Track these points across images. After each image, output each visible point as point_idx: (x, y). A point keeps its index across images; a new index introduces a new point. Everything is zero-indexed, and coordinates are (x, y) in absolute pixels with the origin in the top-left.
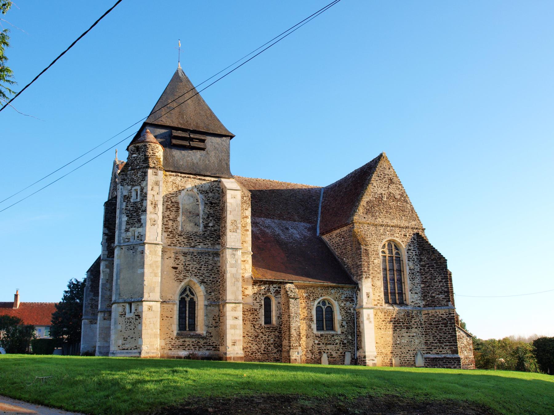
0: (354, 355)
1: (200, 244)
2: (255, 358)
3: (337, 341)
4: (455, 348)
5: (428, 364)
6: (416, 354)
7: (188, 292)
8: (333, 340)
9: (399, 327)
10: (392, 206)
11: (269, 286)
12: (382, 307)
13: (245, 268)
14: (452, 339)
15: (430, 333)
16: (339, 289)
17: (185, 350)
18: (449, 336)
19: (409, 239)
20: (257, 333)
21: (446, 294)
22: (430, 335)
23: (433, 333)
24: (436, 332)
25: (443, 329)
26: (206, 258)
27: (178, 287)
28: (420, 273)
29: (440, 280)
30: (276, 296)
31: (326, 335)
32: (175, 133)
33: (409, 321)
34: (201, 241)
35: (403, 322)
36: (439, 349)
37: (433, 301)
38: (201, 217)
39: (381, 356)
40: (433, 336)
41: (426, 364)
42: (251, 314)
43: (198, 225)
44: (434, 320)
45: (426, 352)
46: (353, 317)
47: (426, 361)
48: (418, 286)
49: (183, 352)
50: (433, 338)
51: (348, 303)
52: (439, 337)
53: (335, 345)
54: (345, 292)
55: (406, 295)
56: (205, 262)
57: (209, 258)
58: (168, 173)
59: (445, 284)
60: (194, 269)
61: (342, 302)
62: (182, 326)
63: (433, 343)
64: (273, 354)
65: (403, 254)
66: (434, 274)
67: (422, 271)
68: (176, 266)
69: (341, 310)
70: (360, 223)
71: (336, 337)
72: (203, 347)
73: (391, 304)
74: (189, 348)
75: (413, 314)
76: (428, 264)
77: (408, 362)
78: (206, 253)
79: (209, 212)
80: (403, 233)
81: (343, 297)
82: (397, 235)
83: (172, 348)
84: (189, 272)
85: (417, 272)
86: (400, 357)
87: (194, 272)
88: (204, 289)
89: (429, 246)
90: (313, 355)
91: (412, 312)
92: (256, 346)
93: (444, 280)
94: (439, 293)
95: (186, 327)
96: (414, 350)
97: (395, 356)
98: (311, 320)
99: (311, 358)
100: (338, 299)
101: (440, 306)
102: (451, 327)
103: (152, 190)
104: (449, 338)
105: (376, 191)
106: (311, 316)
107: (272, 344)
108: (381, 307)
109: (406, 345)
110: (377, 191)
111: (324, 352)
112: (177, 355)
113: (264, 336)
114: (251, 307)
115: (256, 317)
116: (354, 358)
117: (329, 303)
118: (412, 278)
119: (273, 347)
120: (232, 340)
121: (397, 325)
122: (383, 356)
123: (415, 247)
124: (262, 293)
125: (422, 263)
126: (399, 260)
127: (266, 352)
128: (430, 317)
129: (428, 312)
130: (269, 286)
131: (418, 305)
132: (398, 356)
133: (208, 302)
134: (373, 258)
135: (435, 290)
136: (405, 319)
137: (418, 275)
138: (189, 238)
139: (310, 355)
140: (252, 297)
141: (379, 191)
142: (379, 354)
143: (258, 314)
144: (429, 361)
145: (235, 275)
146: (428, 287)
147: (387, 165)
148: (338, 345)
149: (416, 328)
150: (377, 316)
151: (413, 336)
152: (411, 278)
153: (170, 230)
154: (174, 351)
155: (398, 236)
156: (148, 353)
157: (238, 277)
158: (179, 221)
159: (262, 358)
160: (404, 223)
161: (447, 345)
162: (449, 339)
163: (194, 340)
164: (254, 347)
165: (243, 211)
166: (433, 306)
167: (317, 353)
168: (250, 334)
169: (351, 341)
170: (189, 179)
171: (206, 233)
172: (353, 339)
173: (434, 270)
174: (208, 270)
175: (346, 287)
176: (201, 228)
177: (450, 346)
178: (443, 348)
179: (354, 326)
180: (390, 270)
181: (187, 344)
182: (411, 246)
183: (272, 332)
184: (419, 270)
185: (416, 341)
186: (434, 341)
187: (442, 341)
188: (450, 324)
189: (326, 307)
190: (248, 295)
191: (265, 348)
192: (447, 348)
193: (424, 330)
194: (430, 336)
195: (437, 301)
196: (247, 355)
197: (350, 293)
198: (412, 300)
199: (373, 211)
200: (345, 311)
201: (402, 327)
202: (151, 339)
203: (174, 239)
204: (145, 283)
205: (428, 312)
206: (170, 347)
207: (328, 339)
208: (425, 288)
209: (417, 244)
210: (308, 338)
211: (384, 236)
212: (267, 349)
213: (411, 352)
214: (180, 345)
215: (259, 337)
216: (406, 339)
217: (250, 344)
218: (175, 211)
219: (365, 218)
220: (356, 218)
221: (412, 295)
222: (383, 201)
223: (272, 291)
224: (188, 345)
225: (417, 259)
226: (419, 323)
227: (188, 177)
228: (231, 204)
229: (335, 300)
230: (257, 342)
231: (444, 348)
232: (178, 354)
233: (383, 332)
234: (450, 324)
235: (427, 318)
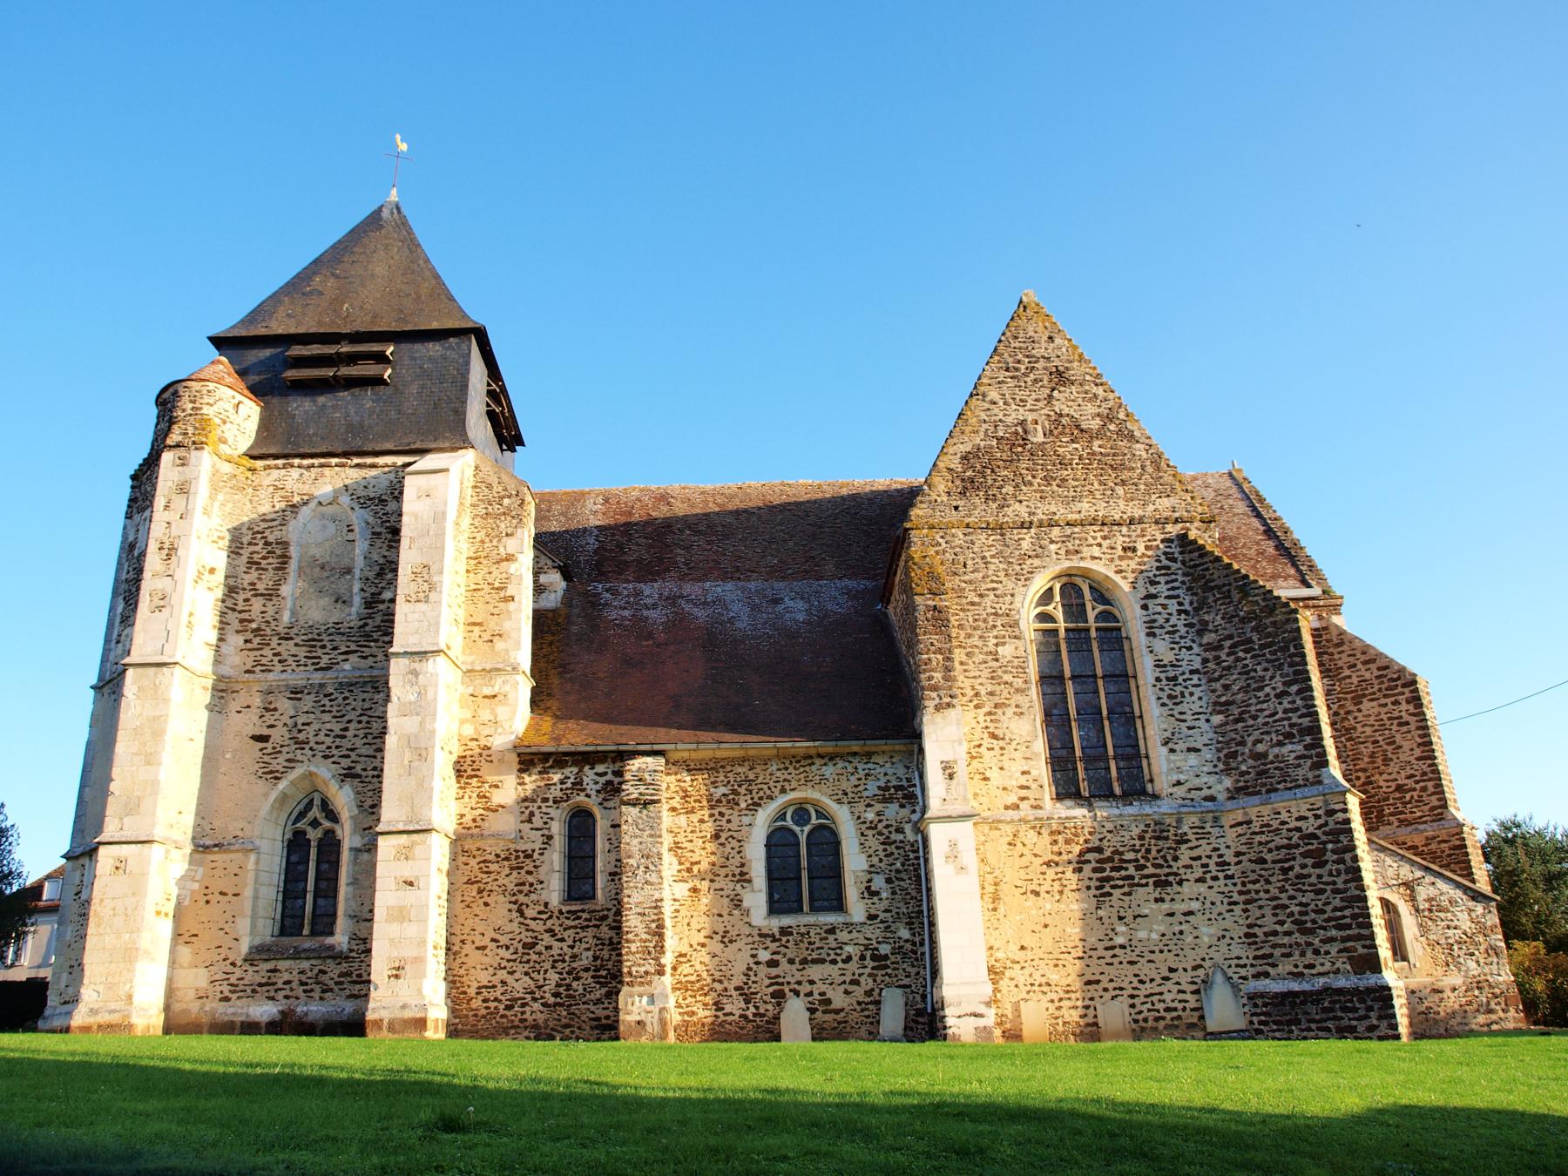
0: (924, 997)
1: (350, 657)
2: (522, 1021)
3: (849, 949)
4: (1364, 947)
5: (1263, 1018)
6: (1203, 981)
7: (315, 812)
8: (834, 945)
9: (1120, 883)
10: (1069, 457)
11: (580, 771)
12: (1040, 813)
13: (496, 717)
14: (1347, 912)
15: (1262, 894)
16: (856, 761)
17: (272, 998)
18: (1337, 903)
19: (1146, 559)
20: (530, 934)
21: (1308, 739)
22: (1260, 903)
23: (1272, 894)
24: (1282, 890)
25: (1309, 876)
26: (364, 700)
27: (266, 795)
28: (1205, 673)
29: (1280, 688)
30: (605, 804)
31: (803, 930)
32: (297, 351)
33: (1164, 857)
34: (353, 647)
35: (1136, 860)
36: (1303, 954)
37: (1260, 774)
38: (357, 577)
39: (1045, 999)
40: (1275, 908)
41: (1255, 1019)
42: (512, 869)
43: (344, 602)
44: (1272, 845)
45: (1252, 971)
46: (912, 855)
47: (1256, 1005)
48: (1202, 723)
49: (265, 1008)
50: (1275, 915)
51: (894, 807)
52: (1296, 909)
53: (840, 965)
54: (878, 770)
55: (1152, 761)
56: (360, 712)
57: (376, 696)
58: (259, 464)
59: (1299, 702)
60: (321, 738)
61: (869, 805)
62: (289, 923)
63: (1275, 933)
64: (593, 1008)
65: (1128, 614)
66: (1255, 671)
67: (1211, 665)
68: (266, 732)
69: (862, 834)
70: (932, 527)
71: (843, 936)
72: (336, 988)
73: (1087, 799)
74: (288, 992)
75: (1185, 828)
76: (1230, 637)
77: (1169, 1016)
78: (366, 683)
79: (385, 557)
80: (1120, 541)
81: (872, 788)
82: (1096, 551)
83: (230, 995)
84: (307, 747)
85: (1192, 672)
86: (1132, 997)
87: (323, 747)
88: (352, 796)
89: (1225, 572)
90: (750, 1006)
91: (1179, 821)
92: (527, 978)
93: (1294, 688)
94: (1281, 738)
95: (302, 926)
96: (1195, 968)
97: (1107, 996)
98: (743, 878)
99: (741, 1016)
100: (850, 795)
101: (1290, 789)
102: (1341, 867)
103: (166, 507)
104: (1335, 909)
105: (1001, 417)
106: (743, 865)
107: (587, 970)
108: (1034, 811)
109: (1157, 949)
110: (1005, 415)
111: (797, 993)
112: (243, 1018)
113: (556, 944)
114: (512, 846)
115: (530, 879)
116: (926, 1009)
117: (820, 815)
118: (1170, 697)
119: (590, 980)
120: (389, 958)
121: (1113, 874)
122: (1055, 996)
123: (1176, 584)
124: (551, 797)
125: (1209, 638)
126: (1113, 637)
127: (564, 997)
128: (1254, 833)
129: (1246, 814)
130: (580, 771)
131: (1206, 792)
132: (1124, 992)
133: (363, 838)
134: (995, 641)
135: (1265, 729)
136: (1148, 851)
137: (1196, 681)
138: (312, 643)
139: (735, 1006)
140: (517, 809)
141: (1013, 416)
142: (1036, 988)
143: (535, 867)
144: (1265, 1005)
145: (412, 739)
146: (1237, 721)
147: (1040, 329)
148: (853, 966)
149: (1200, 880)
150: (1019, 845)
151: (1191, 913)
152: (1164, 695)
153: (254, 626)
154: (238, 1003)
155: (1096, 555)
156: (93, 1012)
157: (423, 746)
158: (283, 595)
159: (546, 1020)
160: (1120, 509)
161: (1331, 940)
162: (1339, 914)
163: (305, 965)
164: (520, 985)
165: (499, 541)
166: (1264, 790)
167: (768, 998)
168: (504, 940)
169: (908, 946)
170: (327, 471)
171: (370, 621)
172: (917, 939)
173: (1252, 657)
174: (370, 737)
175: (883, 752)
176: (354, 610)
177: (1344, 939)
178: (1317, 952)
179: (920, 891)
180: (1073, 678)
181: (281, 981)
182: (1159, 583)
183: (588, 926)
184: (1197, 665)
185: (1204, 929)
186: (1278, 928)
187: (1309, 925)
188: (1334, 852)
189: (807, 829)
190: (503, 807)
191: (558, 985)
192: (1334, 951)
193: (1239, 887)
194: (1260, 907)
195: (1276, 769)
196: (491, 1013)
197: (901, 772)
198: (1175, 778)
199: (990, 482)
200: (882, 838)
201: (1136, 881)
202: (114, 965)
203: (267, 652)
204: (113, 787)
205: (1246, 814)
206: (226, 989)
207: (810, 943)
208: (1228, 728)
209: (1184, 575)
210: (731, 942)
211: (1036, 562)
212: (569, 987)
213: (1184, 978)
214: (260, 985)
215: (539, 948)
216: (1155, 927)
217: (504, 972)
218: (277, 569)
219: (956, 508)
220: (920, 512)
221: (1172, 757)
222: (1029, 447)
223: (591, 788)
224: (285, 983)
225: (1185, 625)
226: (1212, 862)
227: (322, 466)
228: (416, 517)
229: (839, 801)
230: (532, 964)
231: (1322, 951)
232: (247, 1015)
233: (1048, 906)
234: (1334, 852)
235: (1243, 840)
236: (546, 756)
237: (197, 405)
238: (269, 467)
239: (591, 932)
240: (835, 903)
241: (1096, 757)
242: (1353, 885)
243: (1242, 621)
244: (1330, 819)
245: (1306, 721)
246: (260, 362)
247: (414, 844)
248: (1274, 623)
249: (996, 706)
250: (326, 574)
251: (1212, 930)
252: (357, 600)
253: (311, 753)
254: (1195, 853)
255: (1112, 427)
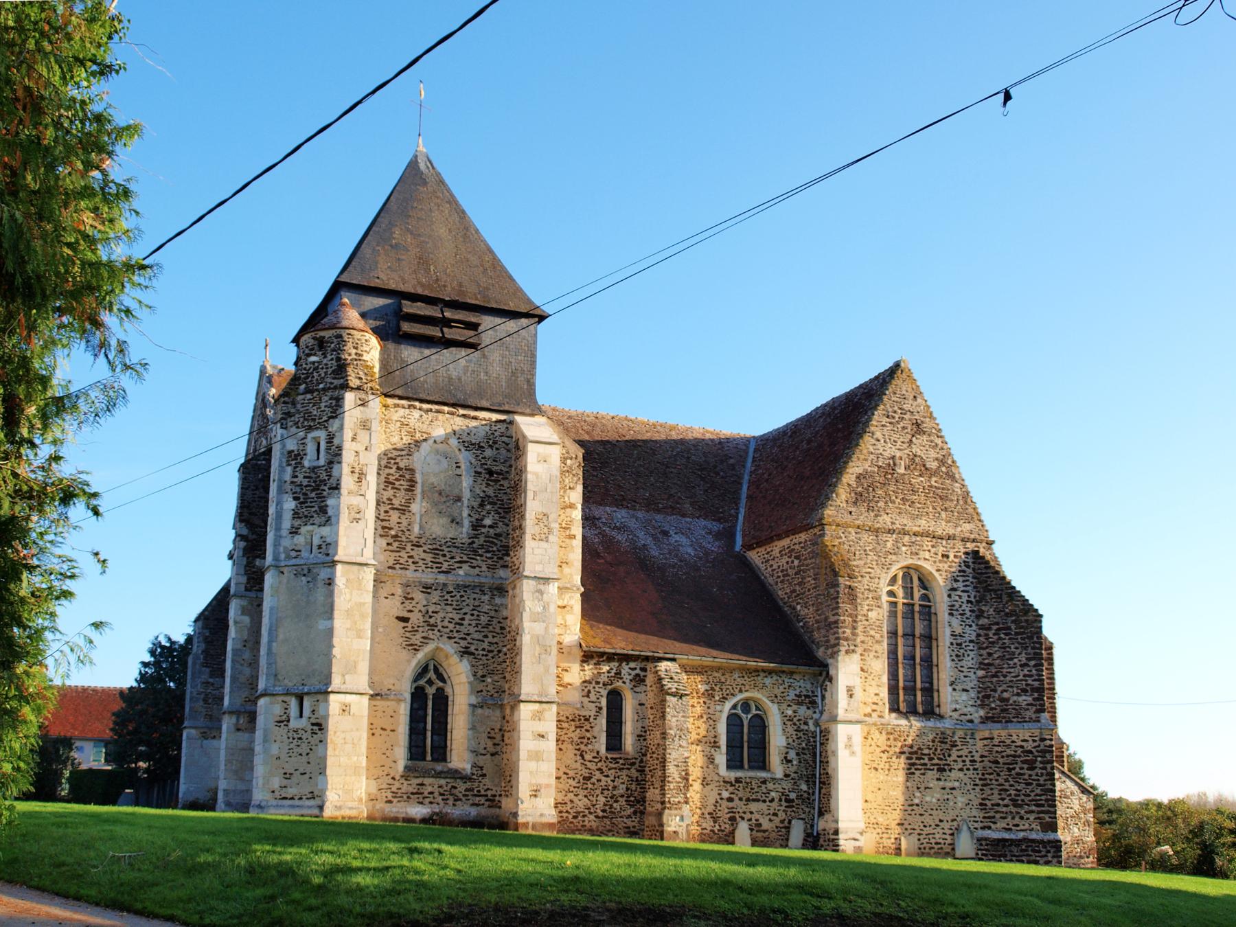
0: (812, 826)
1: (463, 565)
2: (583, 826)
3: (773, 794)
7: (432, 675)
8: (765, 791)
12: (883, 721)
14: (1043, 798)
15: (994, 782)
16: (784, 676)
18: (1038, 791)
21: (1036, 695)
25: (1024, 774)
27: (409, 661)
29: (1024, 661)
31: (748, 780)
34: (465, 558)
36: (1013, 818)
37: (1003, 711)
39: (875, 832)
40: (1001, 790)
41: (980, 852)
42: (576, 727)
44: (1004, 754)
45: (981, 825)
47: (981, 845)
48: (971, 674)
52: (1013, 792)
53: (768, 803)
55: (941, 694)
56: (472, 607)
58: (390, 401)
59: (1034, 672)
60: (446, 623)
61: (789, 706)
62: (416, 750)
63: (998, 805)
64: (625, 820)
65: (938, 598)
67: (982, 639)
68: (406, 615)
70: (838, 525)
71: (770, 786)
72: (464, 799)
74: (432, 800)
75: (956, 738)
76: (997, 624)
77: (936, 847)
80: (941, 550)
81: (792, 695)
82: (927, 555)
84: (436, 629)
86: (919, 834)
87: (448, 630)
91: (954, 733)
92: (586, 799)
93: (1032, 663)
95: (424, 752)
96: (953, 821)
97: (907, 833)
98: (715, 745)
103: (353, 439)
104: (1037, 795)
106: (715, 737)
111: (743, 818)
112: (404, 815)
114: (577, 712)
115: (588, 735)
117: (757, 709)
118: (957, 656)
122: (880, 831)
123: (968, 583)
125: (983, 621)
126: (928, 612)
127: (608, 813)
131: (969, 717)
136: (936, 750)
137: (971, 648)
138: (436, 551)
139: (708, 824)
144: (987, 845)
146: (993, 676)
147: (909, 390)
148: (775, 804)
149: (961, 770)
151: (953, 789)
152: (954, 654)
153: (393, 533)
154: (398, 804)
158: (414, 511)
159: (597, 827)
160: (943, 528)
161: (1032, 812)
163: (443, 782)
164: (581, 803)
165: (565, 492)
167: (727, 821)
168: (571, 773)
169: (806, 795)
170: (440, 416)
171: (476, 540)
172: (811, 791)
176: (464, 530)
177: (1039, 812)
184: (973, 638)
186: (1001, 802)
188: (1041, 762)
189: (749, 716)
191: (605, 805)
193: (980, 776)
194: (992, 789)
197: (809, 686)
198: (954, 706)
203: (403, 554)
204: (336, 651)
206: (390, 795)
209: (973, 578)
211: (894, 557)
212: (611, 806)
213: (946, 825)
214: (412, 793)
215: (593, 780)
217: (572, 794)
218: (406, 490)
221: (954, 693)
223: (627, 678)
227: (438, 411)
228: (536, 474)
229: (772, 701)
233: (882, 778)
234: (1041, 762)
235: (987, 748)
236: (602, 654)
237: (359, 352)
238: (397, 406)
239: (625, 772)
240: (738, 764)
241: (910, 690)
242: (1050, 782)
243: (1007, 615)
244: (1042, 744)
245: (1036, 684)
246: (375, 309)
247: (544, 710)
248: (1027, 621)
249: (865, 650)
250: (444, 499)
251: (963, 800)
252: (466, 523)
253: (438, 634)
254: (960, 753)
255: (944, 469)
